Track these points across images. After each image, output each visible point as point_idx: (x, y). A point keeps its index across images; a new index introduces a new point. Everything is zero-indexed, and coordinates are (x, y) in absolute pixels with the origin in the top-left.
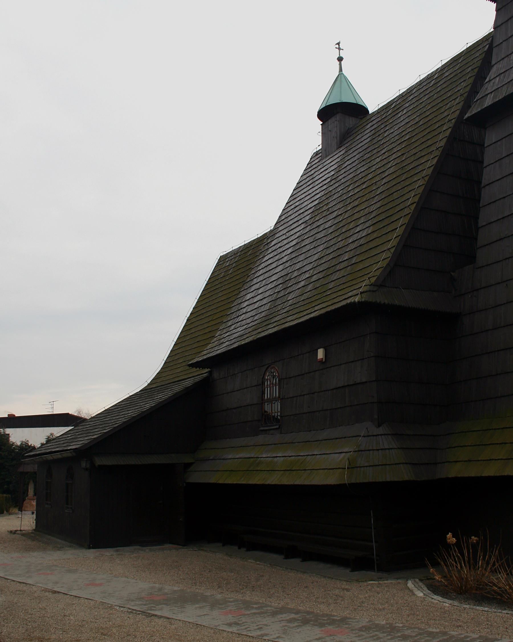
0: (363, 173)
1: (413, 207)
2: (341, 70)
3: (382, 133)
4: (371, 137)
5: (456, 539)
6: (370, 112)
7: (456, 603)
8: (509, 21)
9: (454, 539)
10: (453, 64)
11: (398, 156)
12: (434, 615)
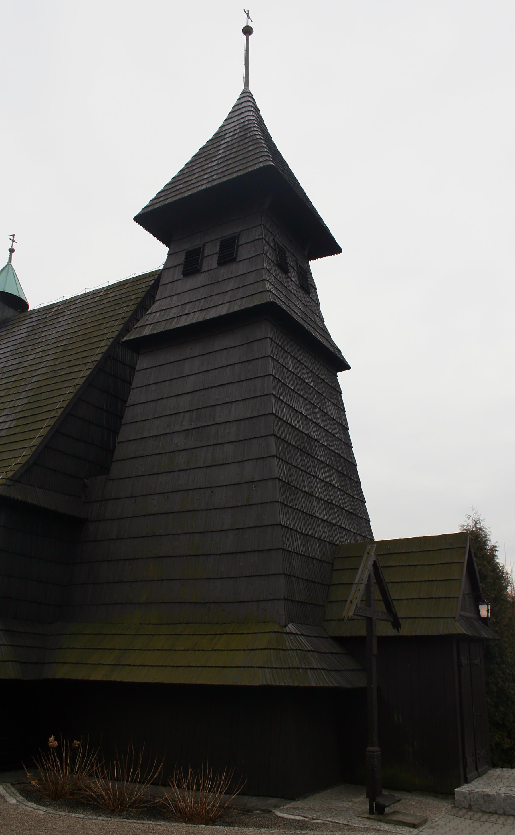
0: (14, 365)
1: (60, 411)
2: (10, 260)
3: (40, 332)
4: (28, 333)
5: (58, 743)
6: (30, 309)
7: (51, 810)
8: (178, 267)
9: (56, 742)
10: (118, 287)
11: (52, 359)
12: (29, 824)
